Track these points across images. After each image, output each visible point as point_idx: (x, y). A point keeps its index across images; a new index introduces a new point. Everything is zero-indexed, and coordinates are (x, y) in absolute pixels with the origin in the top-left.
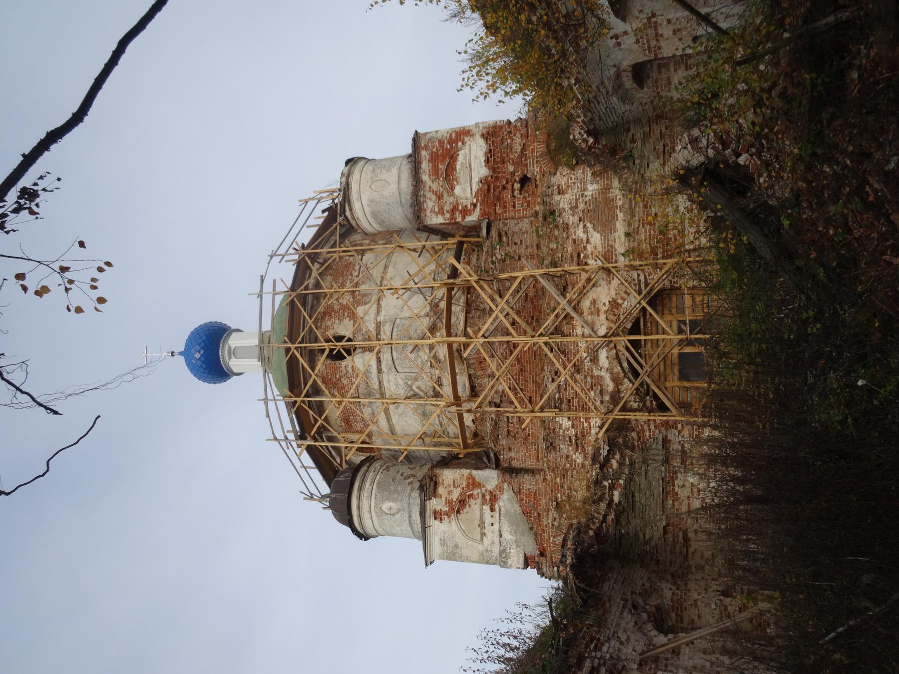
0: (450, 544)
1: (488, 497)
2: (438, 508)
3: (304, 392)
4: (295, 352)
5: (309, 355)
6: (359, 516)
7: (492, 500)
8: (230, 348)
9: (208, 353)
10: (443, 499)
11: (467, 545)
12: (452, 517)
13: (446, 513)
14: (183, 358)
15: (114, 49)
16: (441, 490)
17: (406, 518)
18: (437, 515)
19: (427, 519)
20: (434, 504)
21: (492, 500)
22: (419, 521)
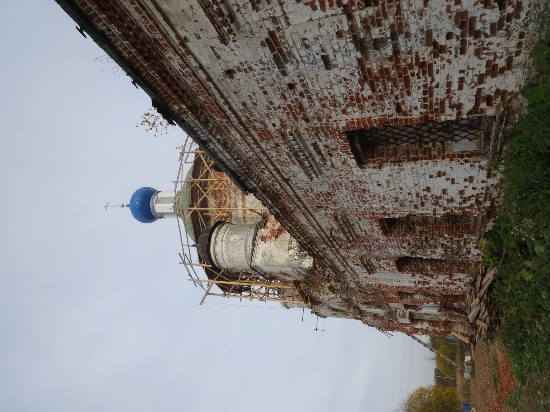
0: (268, 255)
2: (264, 234)
3: (200, 176)
4: (201, 156)
6: (214, 248)
8: (158, 198)
9: (144, 206)
10: (269, 229)
11: (279, 255)
12: (273, 239)
15: (130, 79)
17: (244, 245)
18: (264, 239)
19: (257, 239)
20: (263, 232)
22: (251, 244)
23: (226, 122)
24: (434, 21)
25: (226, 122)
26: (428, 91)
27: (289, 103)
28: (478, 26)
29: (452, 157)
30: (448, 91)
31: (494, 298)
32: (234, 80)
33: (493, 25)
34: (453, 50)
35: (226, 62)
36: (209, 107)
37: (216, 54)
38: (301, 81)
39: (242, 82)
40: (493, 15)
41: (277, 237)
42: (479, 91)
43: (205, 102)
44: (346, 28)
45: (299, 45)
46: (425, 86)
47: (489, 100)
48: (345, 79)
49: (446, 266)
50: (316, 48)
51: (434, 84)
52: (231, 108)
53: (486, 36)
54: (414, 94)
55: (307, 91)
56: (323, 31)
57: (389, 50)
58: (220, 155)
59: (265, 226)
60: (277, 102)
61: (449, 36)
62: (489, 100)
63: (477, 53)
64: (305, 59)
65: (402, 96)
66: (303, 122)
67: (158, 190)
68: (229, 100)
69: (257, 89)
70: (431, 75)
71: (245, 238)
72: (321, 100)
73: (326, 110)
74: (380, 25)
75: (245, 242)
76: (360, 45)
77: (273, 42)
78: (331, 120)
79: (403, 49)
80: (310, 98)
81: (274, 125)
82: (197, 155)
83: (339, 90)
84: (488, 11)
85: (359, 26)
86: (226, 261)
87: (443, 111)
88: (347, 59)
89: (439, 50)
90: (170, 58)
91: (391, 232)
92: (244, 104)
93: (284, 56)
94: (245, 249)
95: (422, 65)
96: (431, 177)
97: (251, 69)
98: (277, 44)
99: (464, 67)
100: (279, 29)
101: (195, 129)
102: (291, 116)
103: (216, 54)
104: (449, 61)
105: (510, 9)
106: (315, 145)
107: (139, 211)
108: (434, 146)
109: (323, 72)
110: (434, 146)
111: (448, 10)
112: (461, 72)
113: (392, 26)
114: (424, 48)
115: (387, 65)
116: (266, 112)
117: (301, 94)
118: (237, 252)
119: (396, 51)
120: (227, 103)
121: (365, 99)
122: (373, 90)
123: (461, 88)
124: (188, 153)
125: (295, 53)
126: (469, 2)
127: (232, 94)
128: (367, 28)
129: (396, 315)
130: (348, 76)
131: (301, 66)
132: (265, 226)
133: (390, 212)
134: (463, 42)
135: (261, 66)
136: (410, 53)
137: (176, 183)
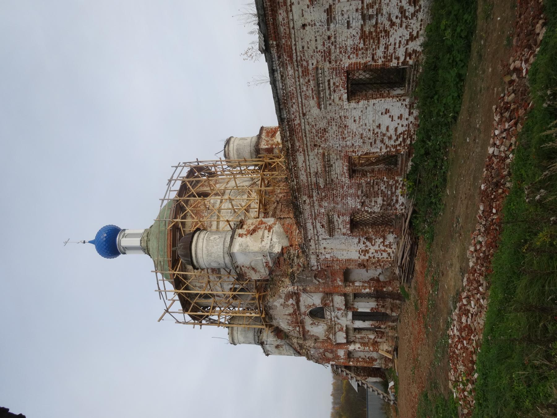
0: (244, 246)
1: (268, 227)
5: (175, 249)
6: (196, 244)
7: (270, 228)
8: (125, 234)
10: (245, 230)
13: (245, 235)
14: (93, 246)
16: (244, 226)
18: (240, 235)
19: (235, 235)
20: (240, 231)
21: (270, 228)
23: (289, 61)
24: (392, 9)
25: (289, 61)
26: (387, 48)
27: (325, 48)
28: (407, 14)
29: (393, 97)
30: (395, 48)
31: (419, 180)
32: (304, 31)
33: (412, 14)
34: (397, 25)
35: (305, 19)
36: (284, 47)
37: (302, 14)
38: (335, 34)
39: (308, 32)
40: (412, 9)
41: (251, 234)
42: (407, 49)
43: (284, 44)
44: (360, 8)
45: (339, 14)
46: (386, 44)
47: (410, 55)
48: (354, 36)
49: (381, 229)
50: (346, 16)
51: (389, 43)
52: (296, 49)
53: (410, 19)
54: (381, 48)
55: (335, 42)
56: (351, 7)
57: (374, 21)
58: (277, 83)
59: (241, 227)
60: (320, 47)
61: (397, 17)
62: (410, 55)
63: (406, 27)
64: (340, 22)
65: (376, 50)
66: (328, 63)
67: (122, 228)
68: (297, 43)
69: (313, 39)
70: (388, 38)
71: (224, 237)
72: (340, 48)
73: (341, 55)
74: (373, 8)
75: (223, 239)
76: (364, 17)
77: (329, 11)
78: (342, 63)
79: (379, 21)
80: (335, 46)
81: (313, 64)
82: (183, 182)
83: (350, 42)
84: (410, 7)
85: (365, 7)
86: (204, 256)
87: (391, 61)
88: (357, 24)
89: (393, 24)
90: (280, 14)
91: (353, 177)
92: (303, 47)
93: (331, 20)
94: (224, 244)
95: (386, 31)
96: (382, 114)
97: (315, 24)
98: (331, 12)
99: (401, 35)
100: (334, 4)
101: (274, 60)
102: (323, 58)
103: (302, 14)
104: (396, 31)
105: (417, 8)
106: (329, 81)
107: (104, 243)
108: (385, 92)
109: (346, 30)
110: (385, 92)
111: (397, 5)
112: (400, 37)
113: (377, 9)
114: (387, 22)
115: (373, 29)
116: (312, 54)
117: (332, 44)
118: (215, 247)
119: (377, 23)
120: (295, 45)
121: (360, 50)
122: (364, 45)
123: (399, 47)
124: (176, 180)
125: (337, 18)
126: (405, 3)
127: (300, 39)
128: (368, 9)
129: (335, 328)
130: (355, 34)
131: (337, 25)
132: (241, 227)
133: (356, 150)
134: (402, 21)
135: (320, 23)
136: (382, 24)
137: (163, 200)
